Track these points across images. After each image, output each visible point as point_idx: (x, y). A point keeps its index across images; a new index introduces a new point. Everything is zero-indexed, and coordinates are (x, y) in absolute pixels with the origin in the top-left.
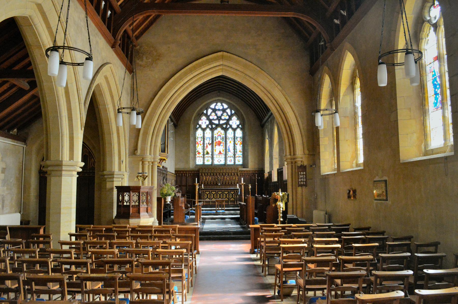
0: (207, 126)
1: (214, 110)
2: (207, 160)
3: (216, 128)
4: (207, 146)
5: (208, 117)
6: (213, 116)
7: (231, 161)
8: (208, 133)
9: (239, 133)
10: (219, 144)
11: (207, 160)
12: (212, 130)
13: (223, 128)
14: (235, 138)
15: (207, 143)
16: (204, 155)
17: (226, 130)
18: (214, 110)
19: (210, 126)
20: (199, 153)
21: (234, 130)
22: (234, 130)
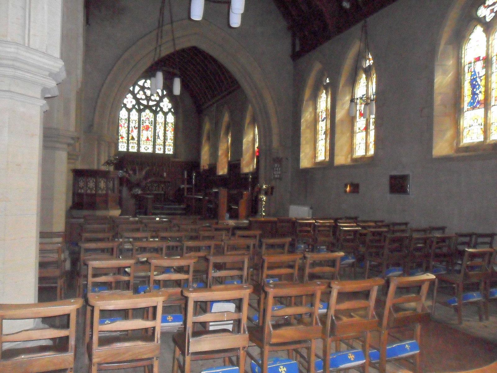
0: (134, 106)
1: (143, 88)
2: (132, 147)
3: (144, 110)
4: (132, 131)
5: (135, 97)
6: (141, 95)
7: (160, 149)
8: (134, 115)
9: (171, 118)
10: (147, 128)
11: (132, 147)
12: (140, 111)
13: (152, 111)
14: (166, 123)
15: (133, 126)
16: (128, 140)
17: (155, 113)
18: (143, 88)
19: (137, 107)
20: (122, 138)
21: (165, 114)
22: (165, 114)
